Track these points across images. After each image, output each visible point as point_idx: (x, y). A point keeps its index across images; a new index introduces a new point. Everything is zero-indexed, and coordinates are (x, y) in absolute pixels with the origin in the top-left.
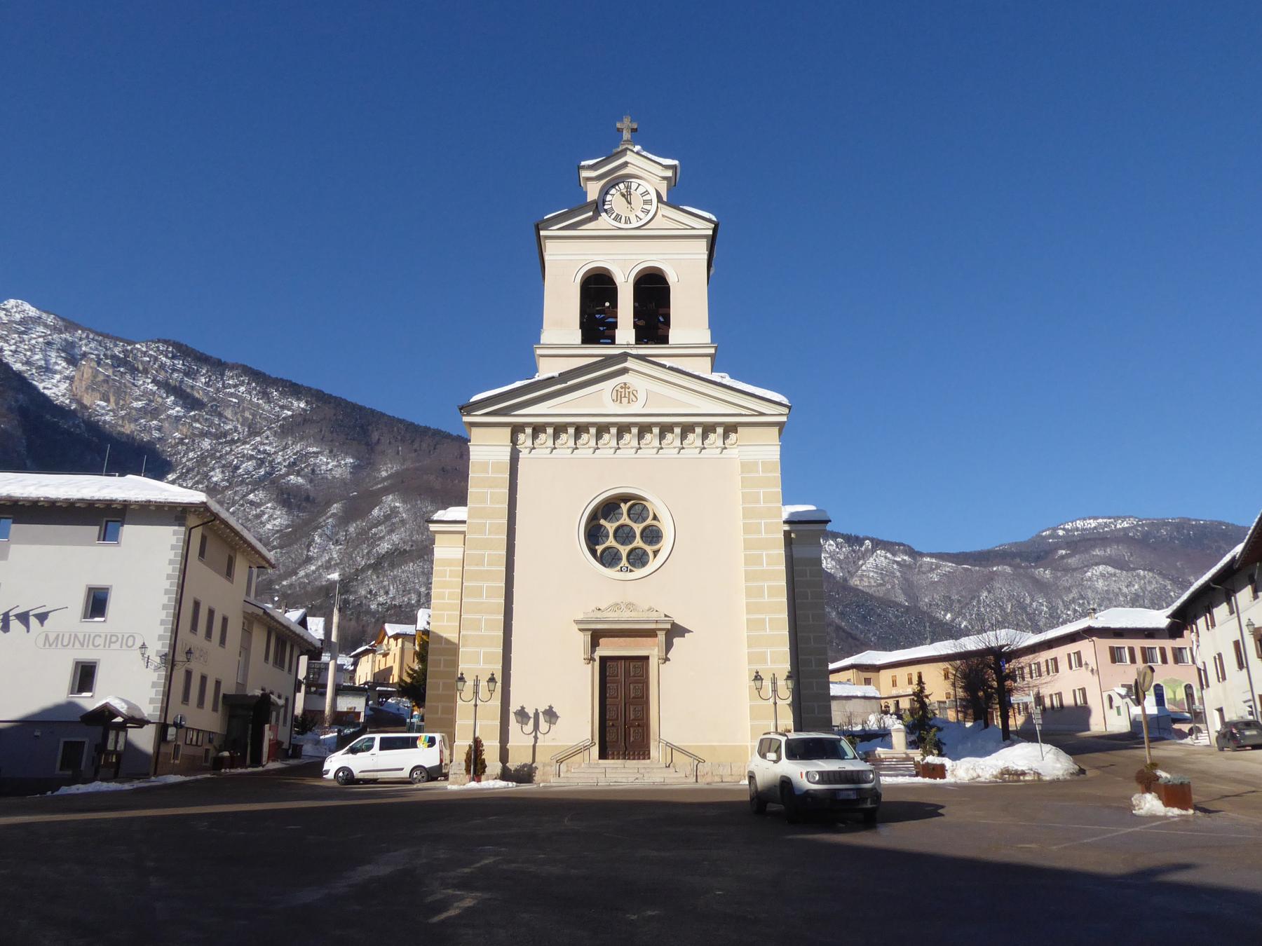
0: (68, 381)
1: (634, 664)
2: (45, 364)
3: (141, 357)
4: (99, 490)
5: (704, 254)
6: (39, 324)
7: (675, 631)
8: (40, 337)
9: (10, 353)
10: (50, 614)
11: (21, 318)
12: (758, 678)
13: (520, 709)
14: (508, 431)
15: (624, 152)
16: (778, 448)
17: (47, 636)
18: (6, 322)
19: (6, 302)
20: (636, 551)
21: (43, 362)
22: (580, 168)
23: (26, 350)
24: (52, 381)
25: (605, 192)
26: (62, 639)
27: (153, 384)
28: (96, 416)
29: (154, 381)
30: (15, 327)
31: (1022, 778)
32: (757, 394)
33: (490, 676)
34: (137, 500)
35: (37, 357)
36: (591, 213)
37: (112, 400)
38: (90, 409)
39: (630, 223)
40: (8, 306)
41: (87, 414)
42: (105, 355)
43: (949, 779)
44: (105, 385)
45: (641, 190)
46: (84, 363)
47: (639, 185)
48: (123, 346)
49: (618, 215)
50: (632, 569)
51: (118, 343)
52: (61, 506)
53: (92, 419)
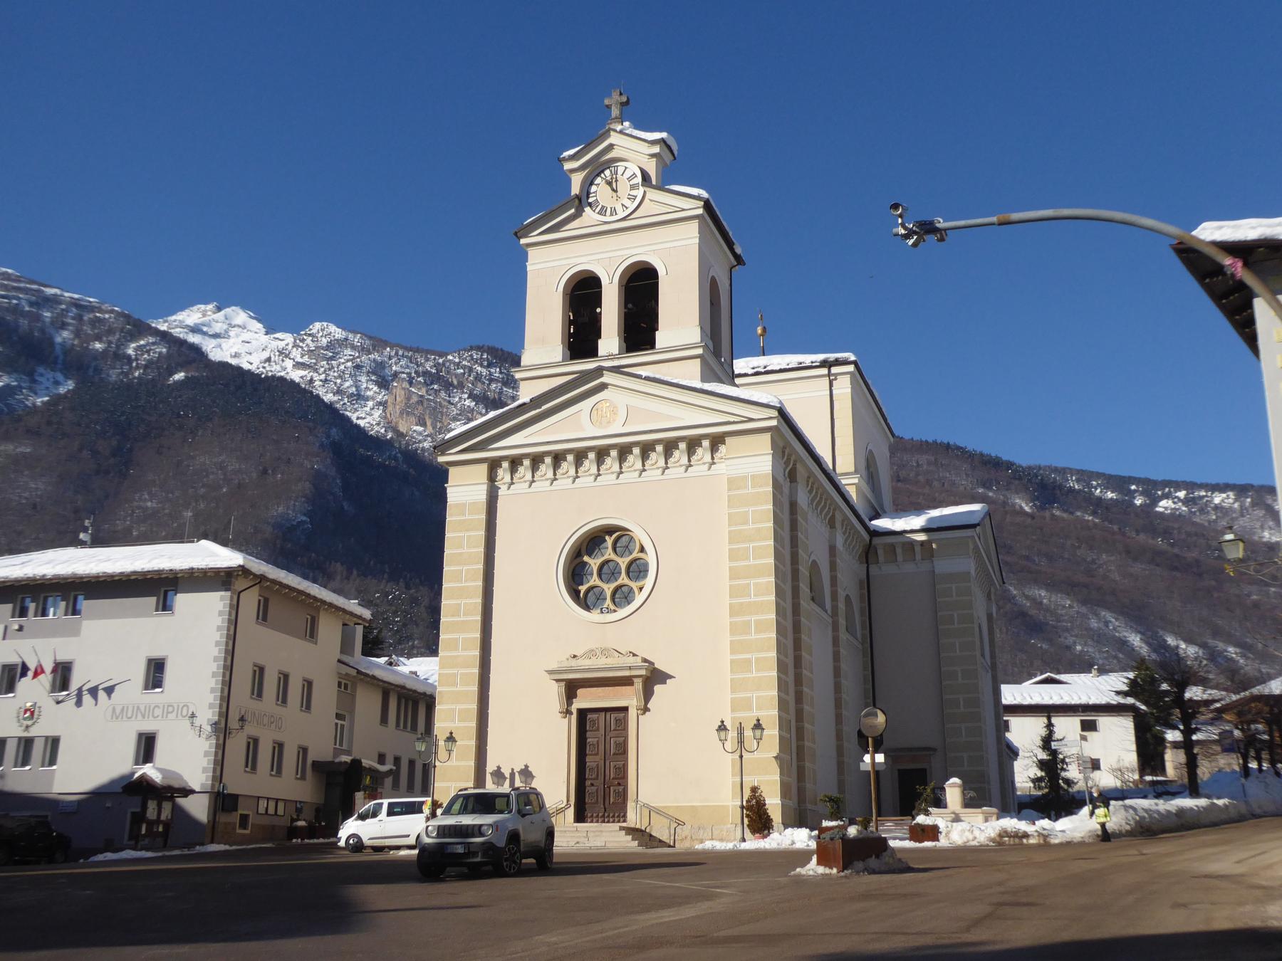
0: (381, 408)
1: (616, 715)
2: (356, 391)
4: (149, 562)
5: (696, 237)
7: (654, 678)
8: (348, 361)
9: (321, 383)
10: (117, 687)
11: (328, 342)
13: (496, 768)
14: (484, 468)
15: (606, 135)
16: (770, 458)
17: (114, 710)
18: (314, 348)
19: (311, 327)
20: (594, 590)
21: (354, 389)
22: (561, 161)
23: (336, 378)
24: (365, 409)
25: (588, 183)
26: (127, 713)
27: (470, 400)
28: (413, 444)
29: (471, 396)
30: (323, 354)
32: (742, 397)
33: (448, 735)
34: (181, 568)
35: (347, 384)
36: (573, 211)
37: (429, 423)
39: (616, 214)
40: (314, 331)
41: (404, 442)
42: (416, 372)
43: (943, 842)
44: (420, 407)
45: (628, 174)
46: (395, 384)
48: (435, 359)
49: (603, 207)
50: (617, 609)
51: (429, 356)
52: (167, 577)
53: (410, 448)
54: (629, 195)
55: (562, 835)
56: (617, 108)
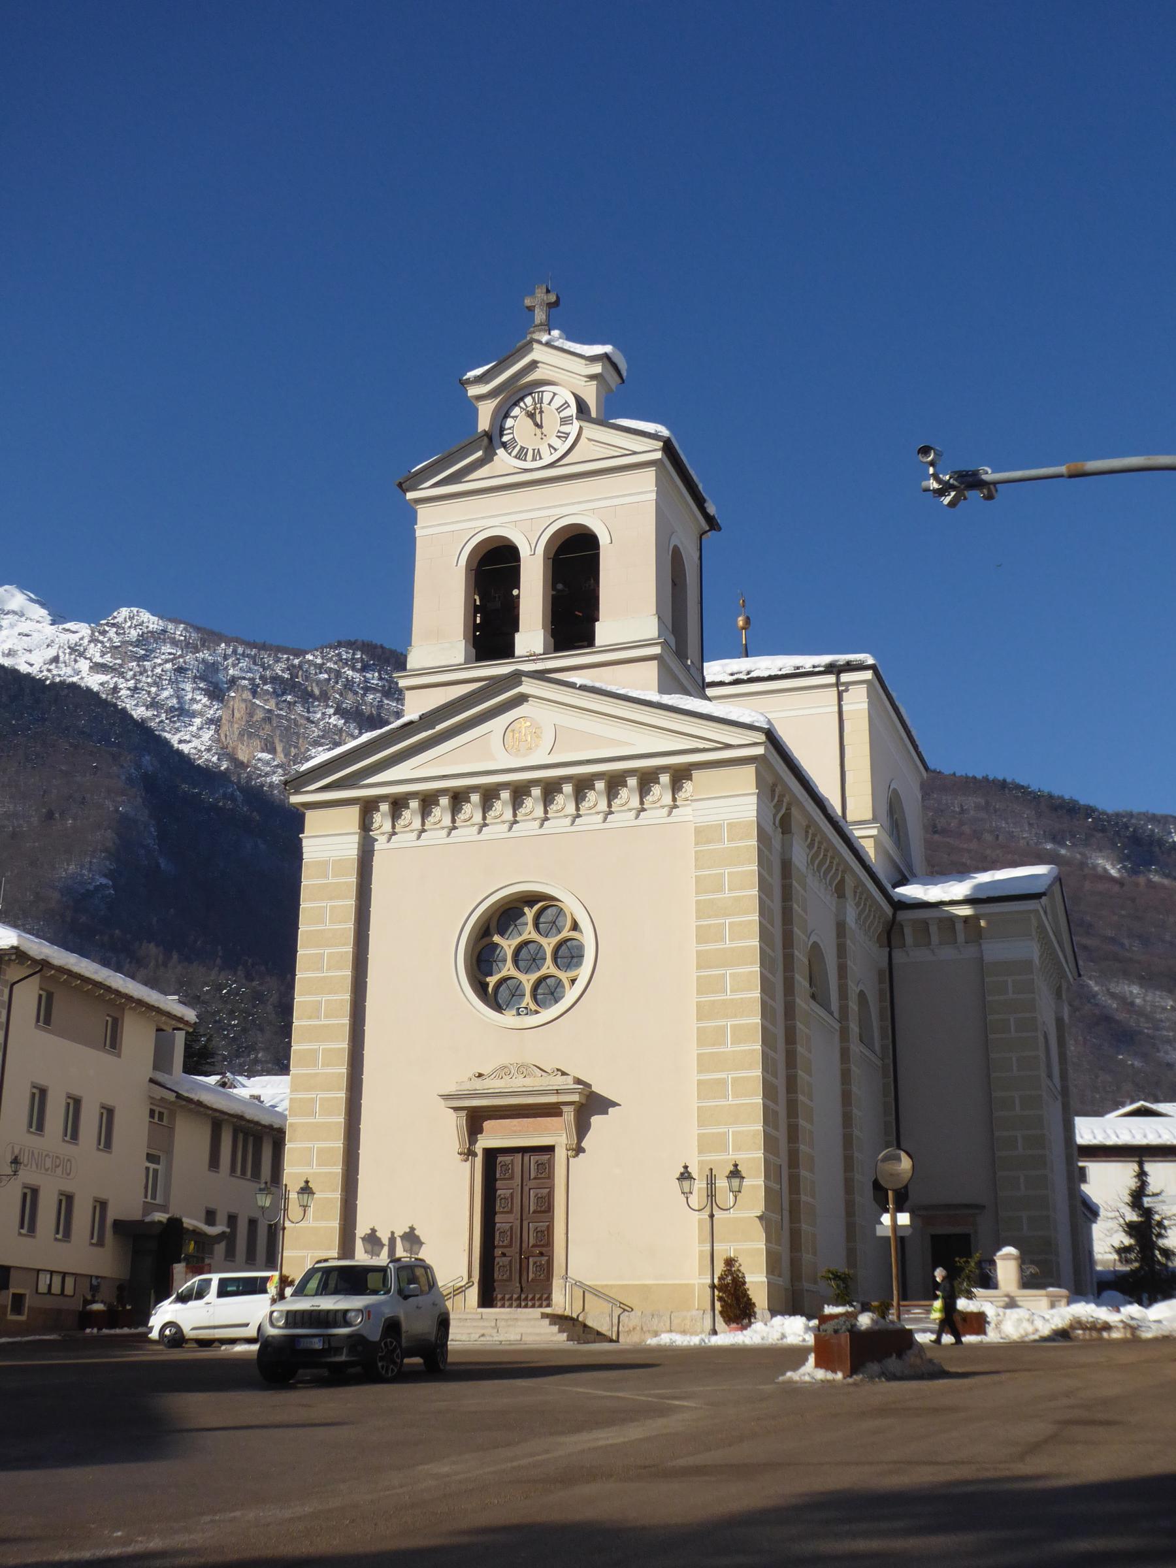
0: (213, 727)
2: (178, 703)
3: (316, 674)
5: (651, 491)
6: (164, 641)
8: (167, 661)
9: (128, 692)
12: (685, 1176)
13: (369, 1232)
14: (354, 812)
15: (527, 347)
16: (754, 799)
18: (119, 644)
19: (115, 614)
21: (175, 701)
22: (465, 384)
23: (149, 685)
24: (190, 728)
25: (502, 414)
29: (339, 711)
30: (131, 651)
31: (1105, 1335)
33: (303, 1184)
35: (165, 694)
36: (480, 453)
37: (279, 748)
38: (248, 767)
39: (541, 458)
40: (120, 620)
42: (261, 677)
43: (992, 1336)
44: (267, 727)
45: (558, 402)
46: (233, 694)
47: (555, 394)
48: (288, 659)
49: (522, 448)
51: (280, 655)
53: (253, 783)
54: (559, 432)
55: (462, 1324)
56: (542, 310)
